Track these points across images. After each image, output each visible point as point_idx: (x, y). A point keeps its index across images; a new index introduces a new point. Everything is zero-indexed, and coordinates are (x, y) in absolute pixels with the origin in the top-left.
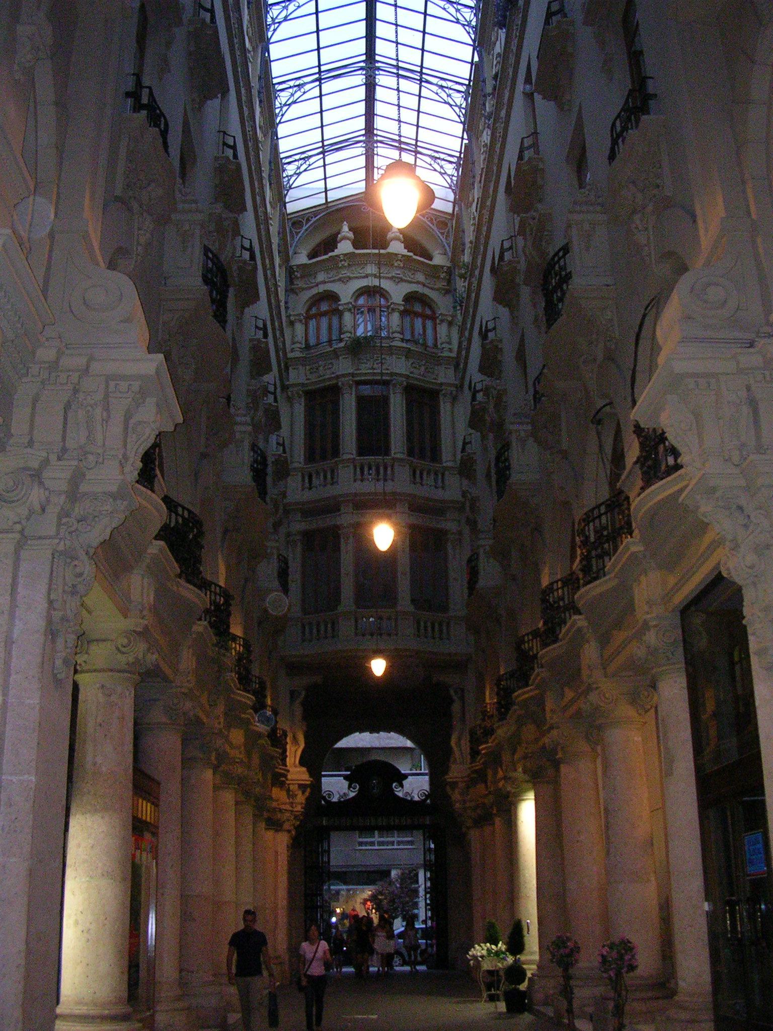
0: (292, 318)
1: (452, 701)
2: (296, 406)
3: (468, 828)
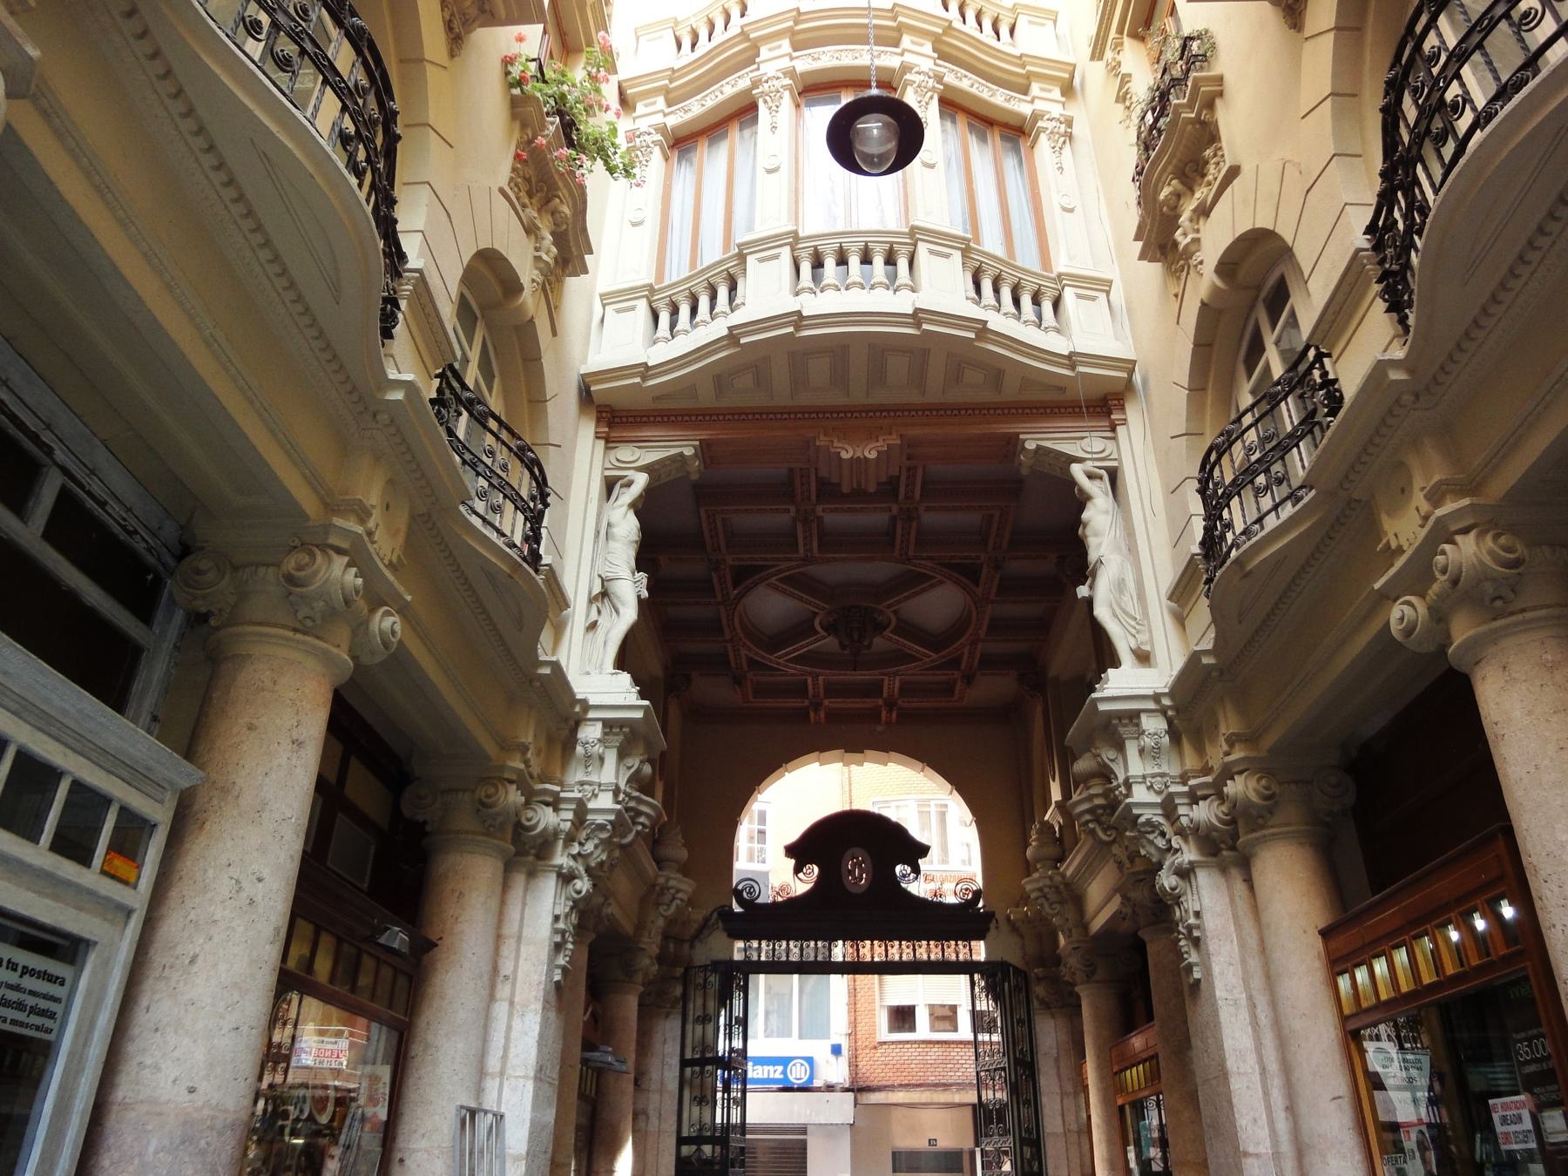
1: (1080, 501)
3: (1185, 873)
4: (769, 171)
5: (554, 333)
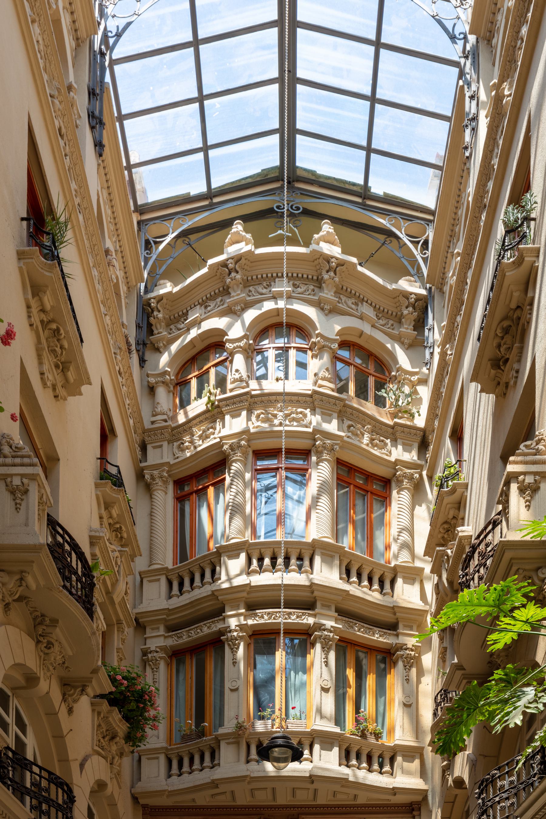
0: (152, 380)
2: (159, 495)
4: (232, 690)
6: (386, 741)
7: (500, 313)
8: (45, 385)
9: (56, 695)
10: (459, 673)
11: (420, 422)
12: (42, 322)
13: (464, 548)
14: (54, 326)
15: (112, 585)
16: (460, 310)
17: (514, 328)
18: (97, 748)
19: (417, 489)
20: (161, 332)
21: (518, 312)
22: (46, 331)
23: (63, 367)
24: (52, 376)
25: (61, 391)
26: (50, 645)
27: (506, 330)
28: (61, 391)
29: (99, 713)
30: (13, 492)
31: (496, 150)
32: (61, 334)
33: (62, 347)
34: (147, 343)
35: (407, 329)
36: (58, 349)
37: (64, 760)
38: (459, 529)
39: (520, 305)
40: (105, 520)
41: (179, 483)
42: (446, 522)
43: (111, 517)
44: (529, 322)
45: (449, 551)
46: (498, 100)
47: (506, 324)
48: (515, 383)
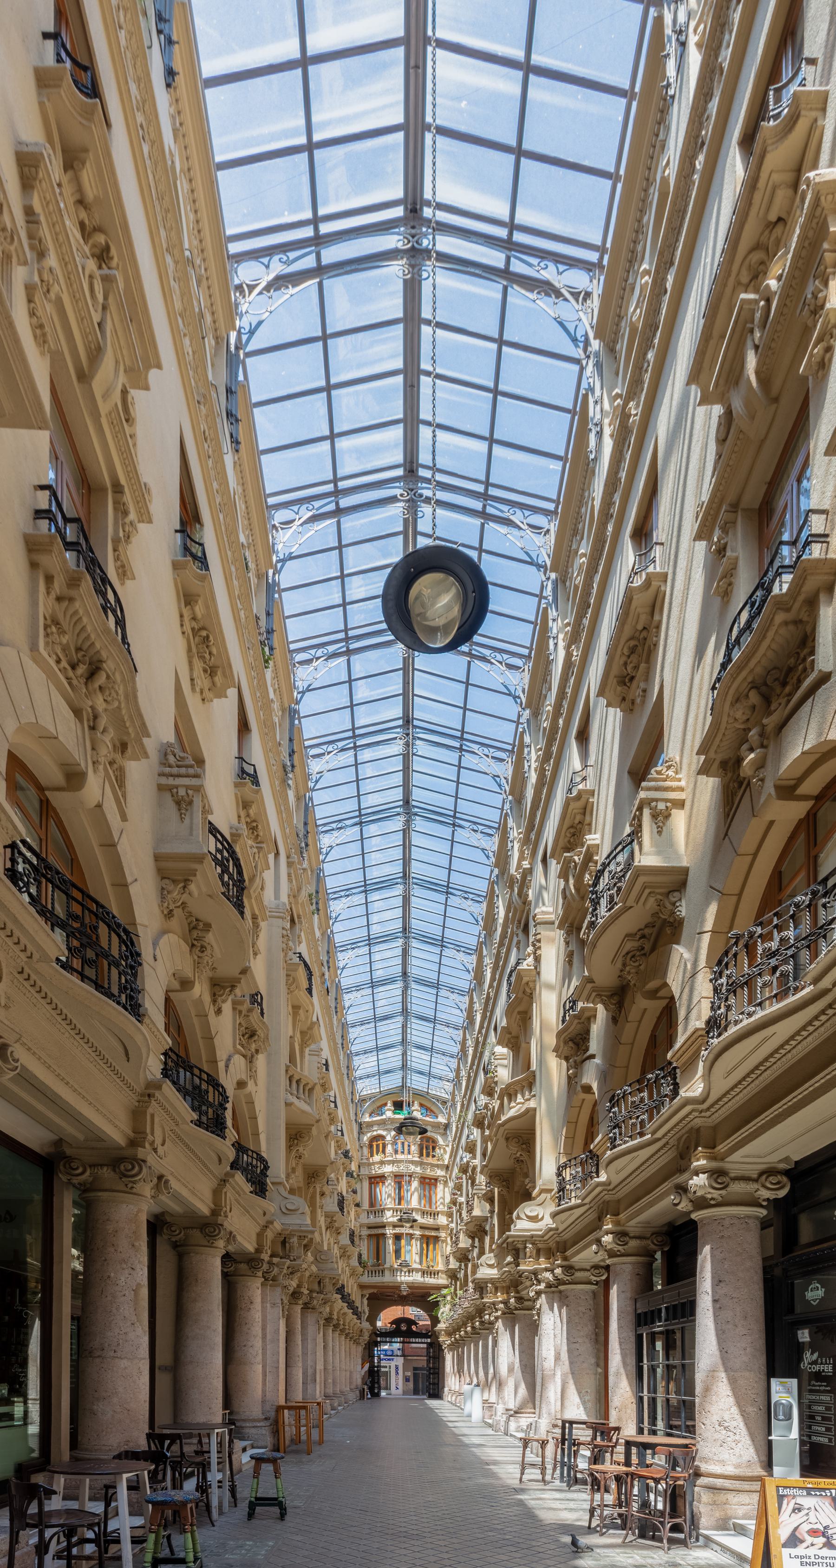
5: (124, 817)
6: (436, 1268)
7: (628, 631)
8: (193, 689)
9: (207, 998)
10: (589, 986)
11: (446, 1163)
12: (193, 629)
13: (825, 225)
14: (204, 633)
15: (89, 358)
16: (586, 613)
17: (640, 648)
18: (239, 1047)
19: (446, 1182)
20: (365, 1130)
21: (644, 634)
22: (197, 639)
23: (211, 671)
24: (203, 682)
25: (207, 694)
26: (203, 949)
27: (633, 650)
28: (207, 694)
29: (240, 1012)
30: (178, 803)
31: (727, 37)
32: (112, 258)
33: (210, 653)
34: (361, 1132)
35: (442, 1131)
36: (207, 656)
37: (214, 1062)
38: (587, 837)
39: (783, 216)
40: (243, 819)
41: (370, 1178)
42: (572, 827)
43: (248, 815)
44: (656, 645)
45: (576, 858)
46: (624, 416)
47: (632, 643)
48: (643, 702)
